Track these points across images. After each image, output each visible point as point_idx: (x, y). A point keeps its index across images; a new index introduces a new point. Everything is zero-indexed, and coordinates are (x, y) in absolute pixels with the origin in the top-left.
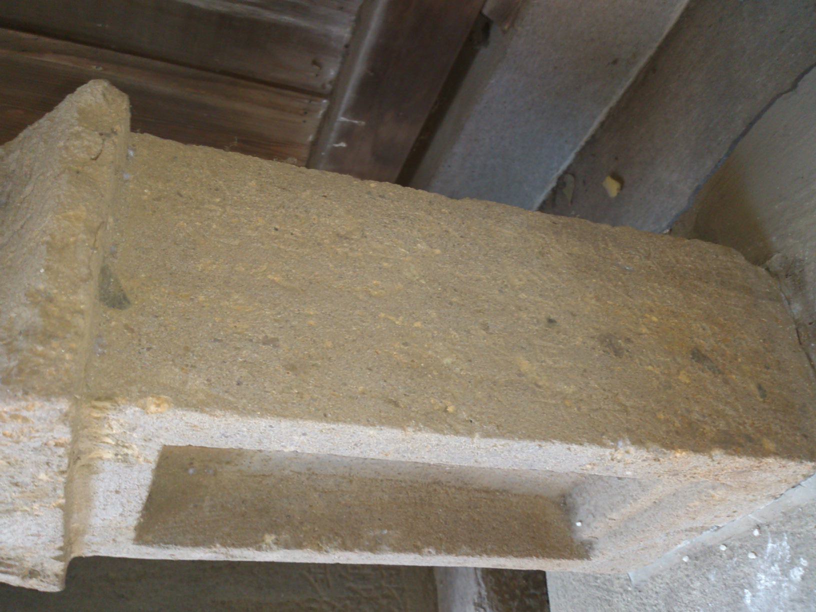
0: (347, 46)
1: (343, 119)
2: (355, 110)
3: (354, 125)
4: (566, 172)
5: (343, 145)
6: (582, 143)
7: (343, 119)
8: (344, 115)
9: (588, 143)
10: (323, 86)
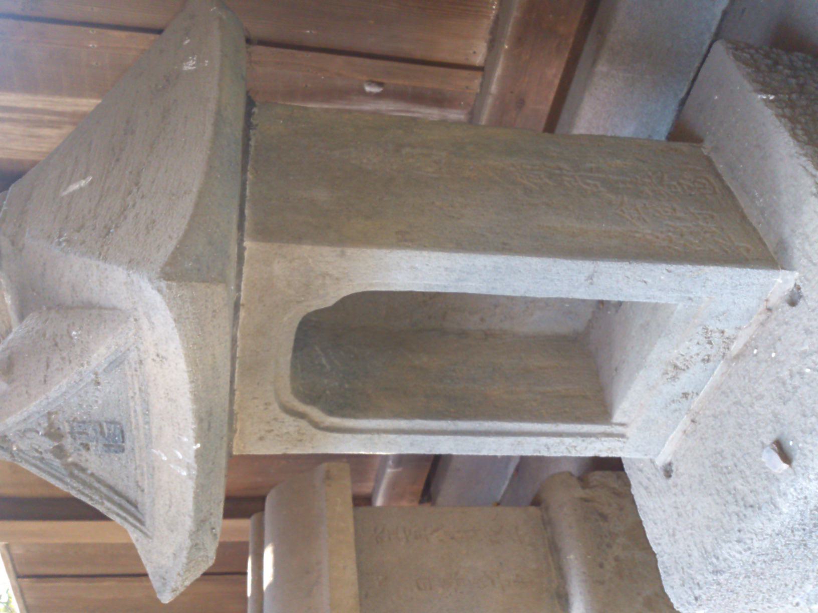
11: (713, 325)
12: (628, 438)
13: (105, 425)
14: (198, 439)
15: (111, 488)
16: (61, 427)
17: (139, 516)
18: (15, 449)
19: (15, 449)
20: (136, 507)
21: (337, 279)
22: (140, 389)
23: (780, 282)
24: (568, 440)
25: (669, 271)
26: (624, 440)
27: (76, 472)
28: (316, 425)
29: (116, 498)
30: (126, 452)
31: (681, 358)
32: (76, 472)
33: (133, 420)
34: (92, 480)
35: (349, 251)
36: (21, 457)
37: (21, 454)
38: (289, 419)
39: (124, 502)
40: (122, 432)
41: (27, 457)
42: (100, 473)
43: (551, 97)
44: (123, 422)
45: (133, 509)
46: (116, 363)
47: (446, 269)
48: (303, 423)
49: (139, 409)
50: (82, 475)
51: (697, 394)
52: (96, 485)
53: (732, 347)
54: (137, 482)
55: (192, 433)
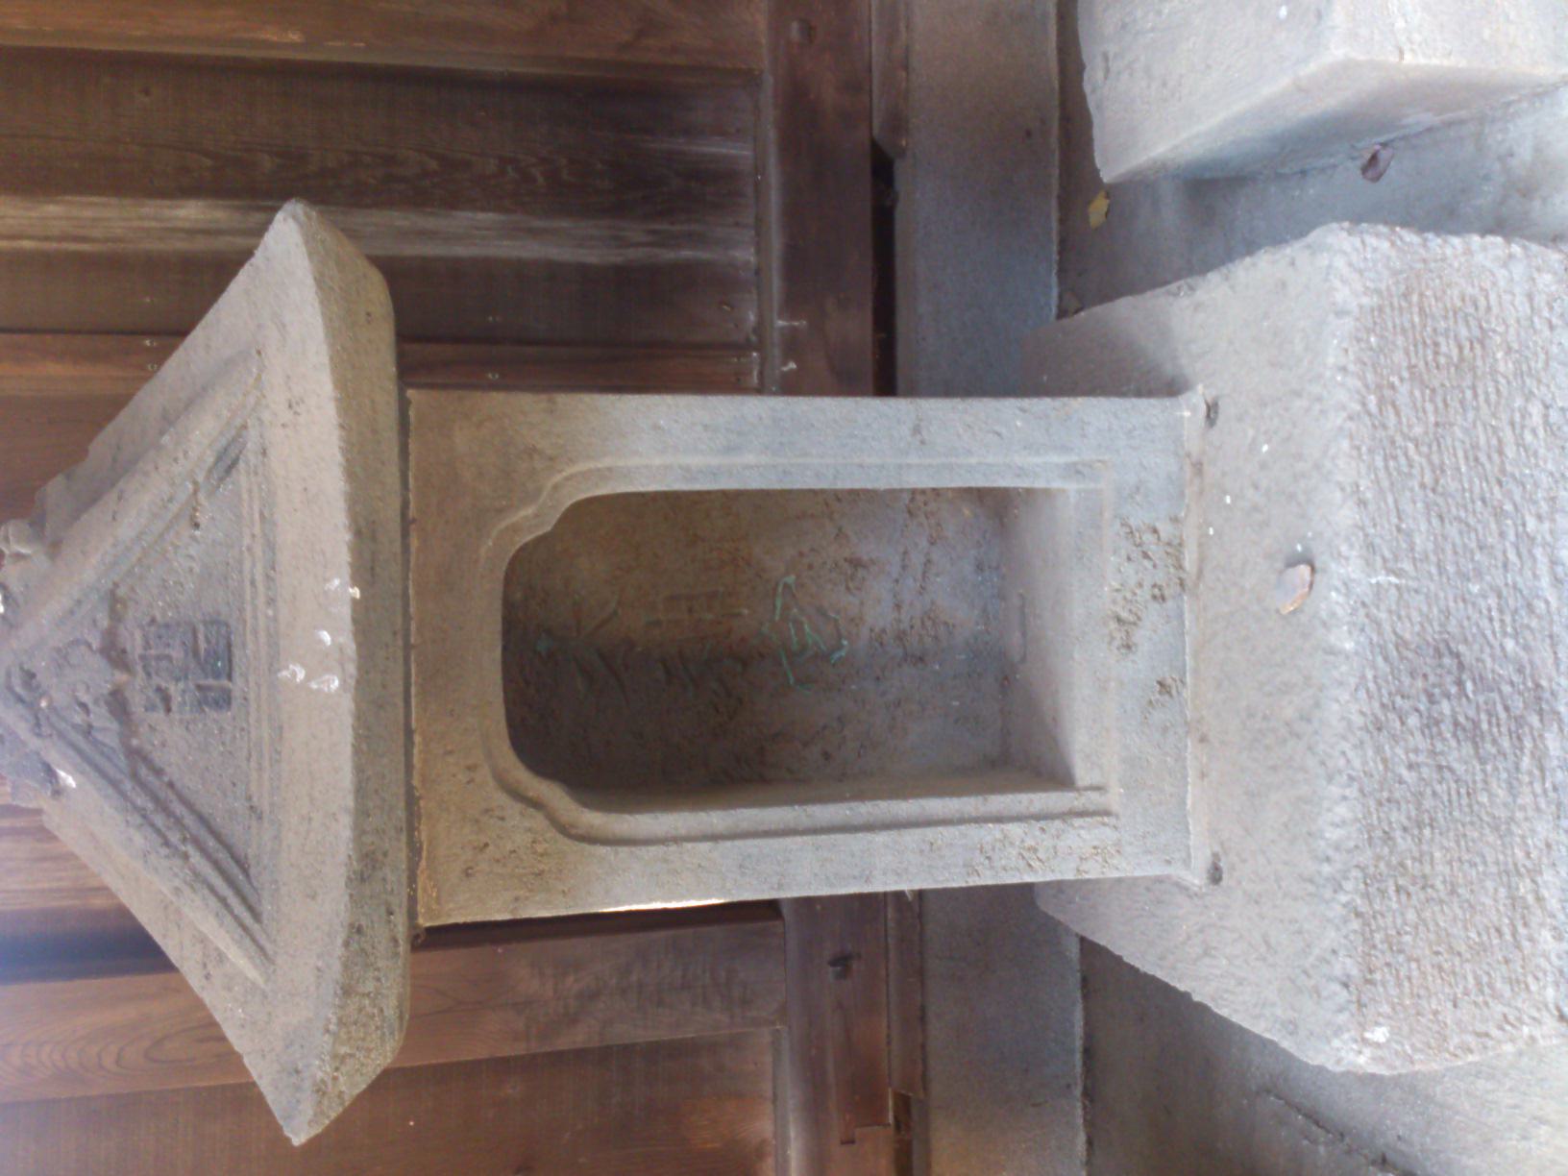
0: (758, 272)
1: (781, 323)
2: (793, 303)
3: (794, 329)
4: (1061, 297)
5: (792, 365)
6: (1055, 257)
7: (781, 323)
8: (780, 317)
9: (1060, 253)
10: (748, 339)
11: (1138, 518)
12: (1117, 817)
13: (201, 628)
14: (356, 580)
15: (202, 819)
16: (129, 648)
17: (247, 889)
18: (44, 704)
19: (44, 704)
20: (246, 872)
21: (551, 459)
22: (262, 514)
23: (1188, 410)
24: (1015, 829)
25: (1023, 410)
26: (1112, 821)
27: (143, 771)
28: (565, 830)
29: (211, 843)
30: (235, 704)
31: (1119, 597)
32: (143, 771)
33: (248, 615)
34: (172, 796)
35: (562, 399)
36: (52, 726)
37: (54, 719)
38: (513, 808)
39: (222, 856)
40: (229, 646)
41: (62, 725)
42: (190, 783)
43: (824, 837)
44: (233, 623)
45: (235, 870)
46: (227, 463)
47: (706, 427)
48: (538, 821)
49: (259, 578)
50: (151, 778)
51: (1183, 683)
52: (179, 809)
53: (1187, 565)
54: (249, 798)
55: (346, 571)
